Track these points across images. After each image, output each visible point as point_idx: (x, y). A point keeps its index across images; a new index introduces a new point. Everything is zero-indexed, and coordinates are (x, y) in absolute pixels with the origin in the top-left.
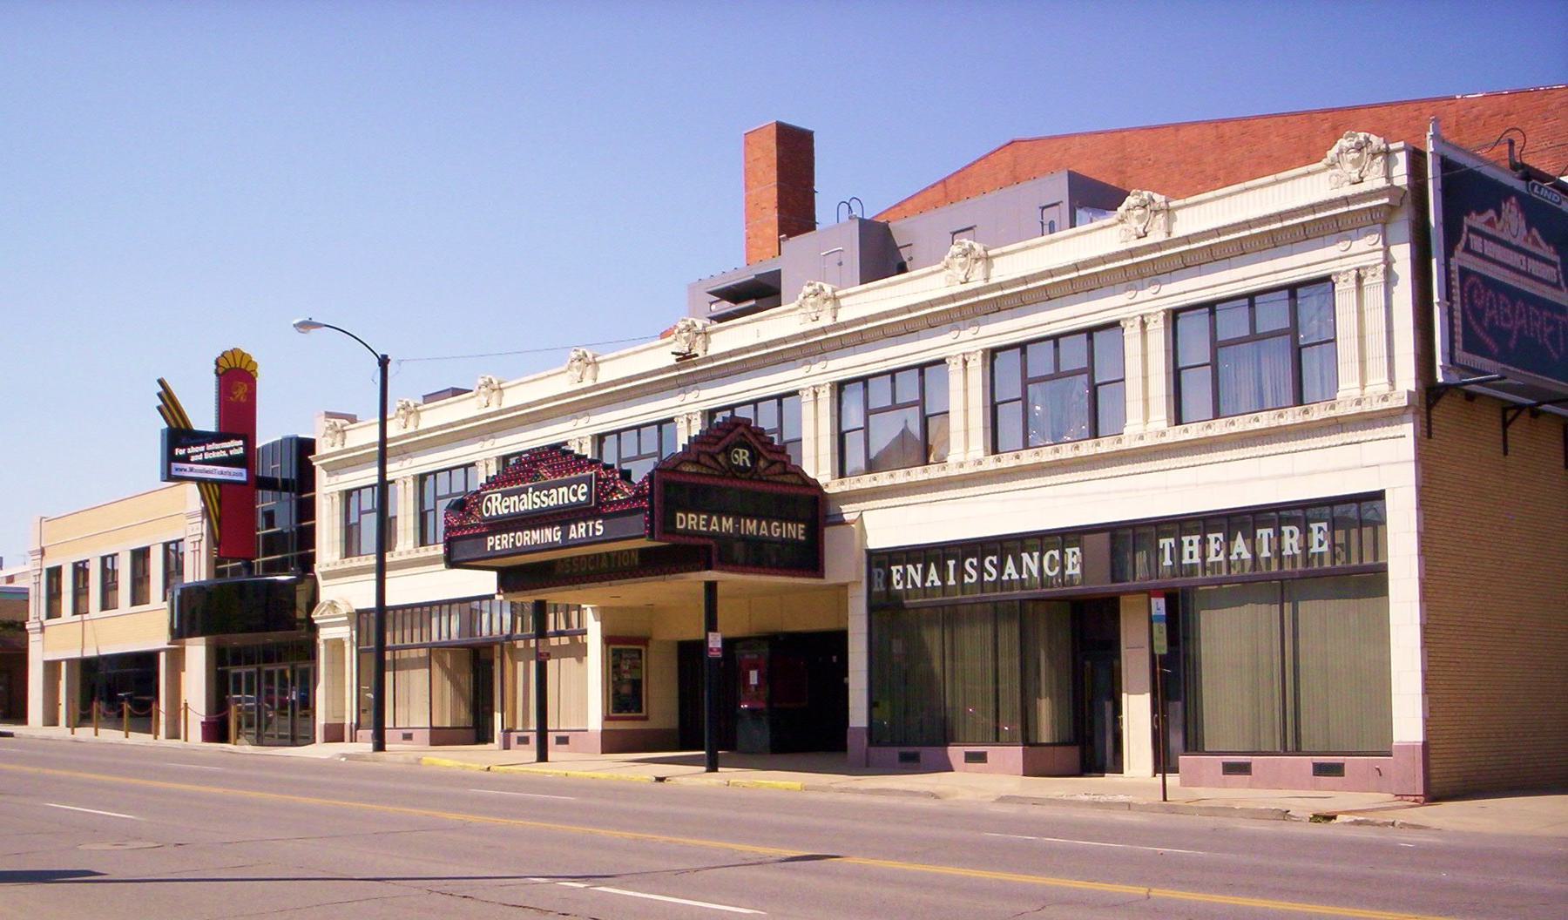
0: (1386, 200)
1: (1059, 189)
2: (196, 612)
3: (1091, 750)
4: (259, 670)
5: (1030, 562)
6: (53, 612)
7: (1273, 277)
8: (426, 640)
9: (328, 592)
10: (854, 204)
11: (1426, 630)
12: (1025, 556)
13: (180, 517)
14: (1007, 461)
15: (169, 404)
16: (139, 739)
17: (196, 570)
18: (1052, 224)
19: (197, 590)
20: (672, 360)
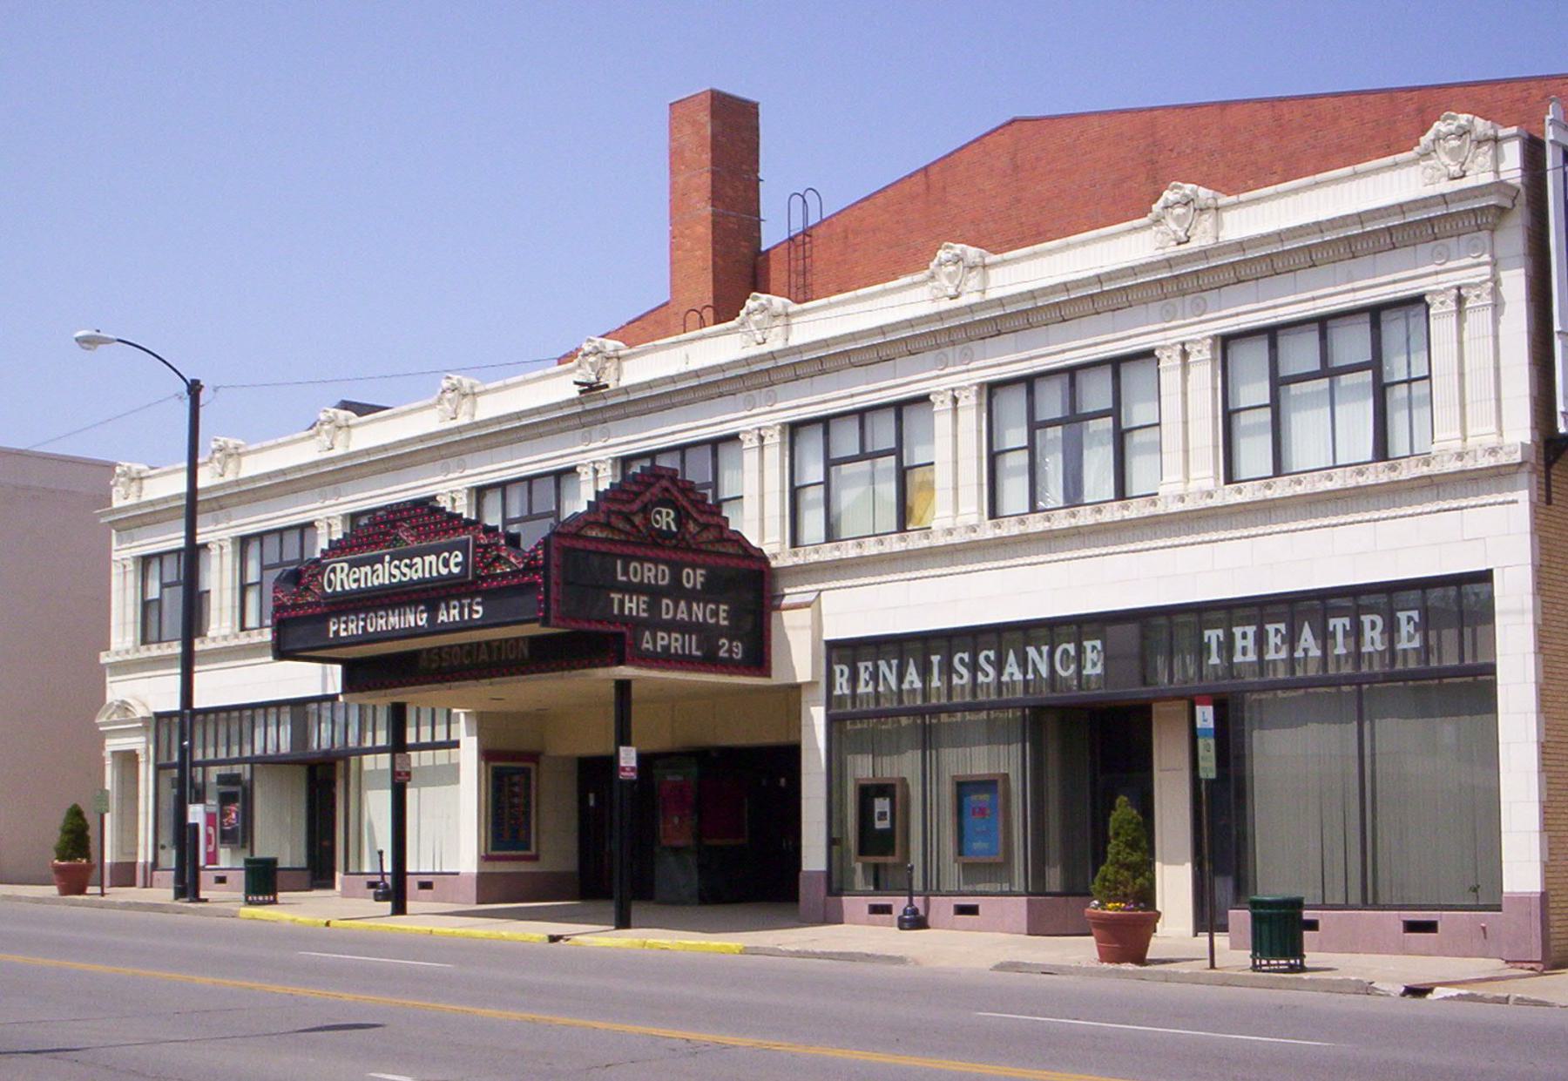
9: (117, 689)
10: (810, 196)
11: (1544, 749)
12: (1032, 652)
20: (574, 392)
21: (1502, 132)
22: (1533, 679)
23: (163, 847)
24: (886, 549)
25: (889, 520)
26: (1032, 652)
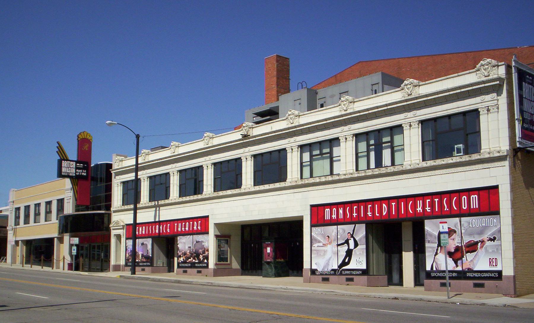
0: (498, 82)
1: (377, 78)
2: (69, 225)
4: (90, 245)
6: (17, 223)
7: (446, 112)
9: (115, 217)
10: (304, 83)
11: (514, 235)
13: (65, 190)
14: (383, 171)
15: (61, 151)
16: (46, 269)
17: (69, 209)
18: (376, 90)
19: (67, 217)
20: (240, 137)
21: (500, 64)
22: (510, 215)
24: (327, 179)
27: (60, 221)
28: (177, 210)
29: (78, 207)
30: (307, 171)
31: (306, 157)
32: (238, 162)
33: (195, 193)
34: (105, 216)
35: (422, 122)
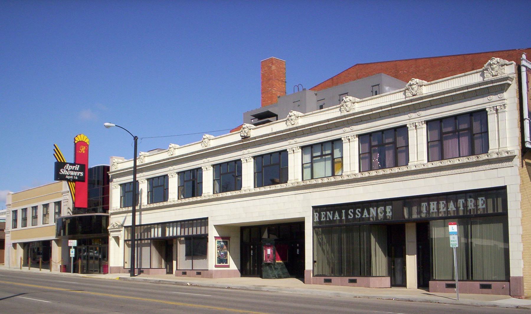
3: (398, 279)
5: (373, 211)
6: (15, 226)
7: (476, 107)
8: (149, 237)
10: (300, 87)
12: (371, 209)
15: (56, 152)
16: (44, 271)
18: (376, 92)
23: (126, 263)
24: (329, 181)
25: (329, 173)
26: (371, 209)
27: (57, 224)
28: (176, 211)
29: (76, 209)
30: (307, 172)
31: (307, 158)
32: (238, 163)
33: (193, 196)
34: (103, 218)
35: (360, 137)
